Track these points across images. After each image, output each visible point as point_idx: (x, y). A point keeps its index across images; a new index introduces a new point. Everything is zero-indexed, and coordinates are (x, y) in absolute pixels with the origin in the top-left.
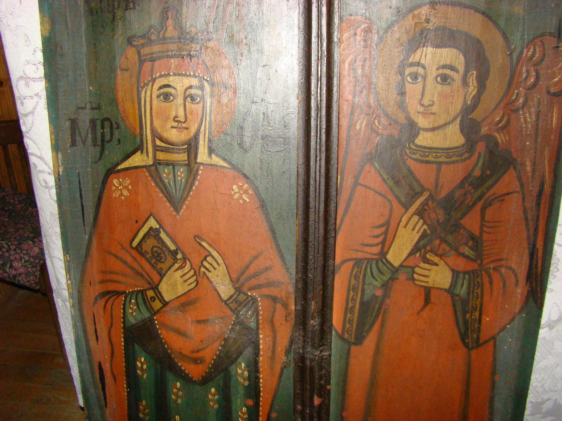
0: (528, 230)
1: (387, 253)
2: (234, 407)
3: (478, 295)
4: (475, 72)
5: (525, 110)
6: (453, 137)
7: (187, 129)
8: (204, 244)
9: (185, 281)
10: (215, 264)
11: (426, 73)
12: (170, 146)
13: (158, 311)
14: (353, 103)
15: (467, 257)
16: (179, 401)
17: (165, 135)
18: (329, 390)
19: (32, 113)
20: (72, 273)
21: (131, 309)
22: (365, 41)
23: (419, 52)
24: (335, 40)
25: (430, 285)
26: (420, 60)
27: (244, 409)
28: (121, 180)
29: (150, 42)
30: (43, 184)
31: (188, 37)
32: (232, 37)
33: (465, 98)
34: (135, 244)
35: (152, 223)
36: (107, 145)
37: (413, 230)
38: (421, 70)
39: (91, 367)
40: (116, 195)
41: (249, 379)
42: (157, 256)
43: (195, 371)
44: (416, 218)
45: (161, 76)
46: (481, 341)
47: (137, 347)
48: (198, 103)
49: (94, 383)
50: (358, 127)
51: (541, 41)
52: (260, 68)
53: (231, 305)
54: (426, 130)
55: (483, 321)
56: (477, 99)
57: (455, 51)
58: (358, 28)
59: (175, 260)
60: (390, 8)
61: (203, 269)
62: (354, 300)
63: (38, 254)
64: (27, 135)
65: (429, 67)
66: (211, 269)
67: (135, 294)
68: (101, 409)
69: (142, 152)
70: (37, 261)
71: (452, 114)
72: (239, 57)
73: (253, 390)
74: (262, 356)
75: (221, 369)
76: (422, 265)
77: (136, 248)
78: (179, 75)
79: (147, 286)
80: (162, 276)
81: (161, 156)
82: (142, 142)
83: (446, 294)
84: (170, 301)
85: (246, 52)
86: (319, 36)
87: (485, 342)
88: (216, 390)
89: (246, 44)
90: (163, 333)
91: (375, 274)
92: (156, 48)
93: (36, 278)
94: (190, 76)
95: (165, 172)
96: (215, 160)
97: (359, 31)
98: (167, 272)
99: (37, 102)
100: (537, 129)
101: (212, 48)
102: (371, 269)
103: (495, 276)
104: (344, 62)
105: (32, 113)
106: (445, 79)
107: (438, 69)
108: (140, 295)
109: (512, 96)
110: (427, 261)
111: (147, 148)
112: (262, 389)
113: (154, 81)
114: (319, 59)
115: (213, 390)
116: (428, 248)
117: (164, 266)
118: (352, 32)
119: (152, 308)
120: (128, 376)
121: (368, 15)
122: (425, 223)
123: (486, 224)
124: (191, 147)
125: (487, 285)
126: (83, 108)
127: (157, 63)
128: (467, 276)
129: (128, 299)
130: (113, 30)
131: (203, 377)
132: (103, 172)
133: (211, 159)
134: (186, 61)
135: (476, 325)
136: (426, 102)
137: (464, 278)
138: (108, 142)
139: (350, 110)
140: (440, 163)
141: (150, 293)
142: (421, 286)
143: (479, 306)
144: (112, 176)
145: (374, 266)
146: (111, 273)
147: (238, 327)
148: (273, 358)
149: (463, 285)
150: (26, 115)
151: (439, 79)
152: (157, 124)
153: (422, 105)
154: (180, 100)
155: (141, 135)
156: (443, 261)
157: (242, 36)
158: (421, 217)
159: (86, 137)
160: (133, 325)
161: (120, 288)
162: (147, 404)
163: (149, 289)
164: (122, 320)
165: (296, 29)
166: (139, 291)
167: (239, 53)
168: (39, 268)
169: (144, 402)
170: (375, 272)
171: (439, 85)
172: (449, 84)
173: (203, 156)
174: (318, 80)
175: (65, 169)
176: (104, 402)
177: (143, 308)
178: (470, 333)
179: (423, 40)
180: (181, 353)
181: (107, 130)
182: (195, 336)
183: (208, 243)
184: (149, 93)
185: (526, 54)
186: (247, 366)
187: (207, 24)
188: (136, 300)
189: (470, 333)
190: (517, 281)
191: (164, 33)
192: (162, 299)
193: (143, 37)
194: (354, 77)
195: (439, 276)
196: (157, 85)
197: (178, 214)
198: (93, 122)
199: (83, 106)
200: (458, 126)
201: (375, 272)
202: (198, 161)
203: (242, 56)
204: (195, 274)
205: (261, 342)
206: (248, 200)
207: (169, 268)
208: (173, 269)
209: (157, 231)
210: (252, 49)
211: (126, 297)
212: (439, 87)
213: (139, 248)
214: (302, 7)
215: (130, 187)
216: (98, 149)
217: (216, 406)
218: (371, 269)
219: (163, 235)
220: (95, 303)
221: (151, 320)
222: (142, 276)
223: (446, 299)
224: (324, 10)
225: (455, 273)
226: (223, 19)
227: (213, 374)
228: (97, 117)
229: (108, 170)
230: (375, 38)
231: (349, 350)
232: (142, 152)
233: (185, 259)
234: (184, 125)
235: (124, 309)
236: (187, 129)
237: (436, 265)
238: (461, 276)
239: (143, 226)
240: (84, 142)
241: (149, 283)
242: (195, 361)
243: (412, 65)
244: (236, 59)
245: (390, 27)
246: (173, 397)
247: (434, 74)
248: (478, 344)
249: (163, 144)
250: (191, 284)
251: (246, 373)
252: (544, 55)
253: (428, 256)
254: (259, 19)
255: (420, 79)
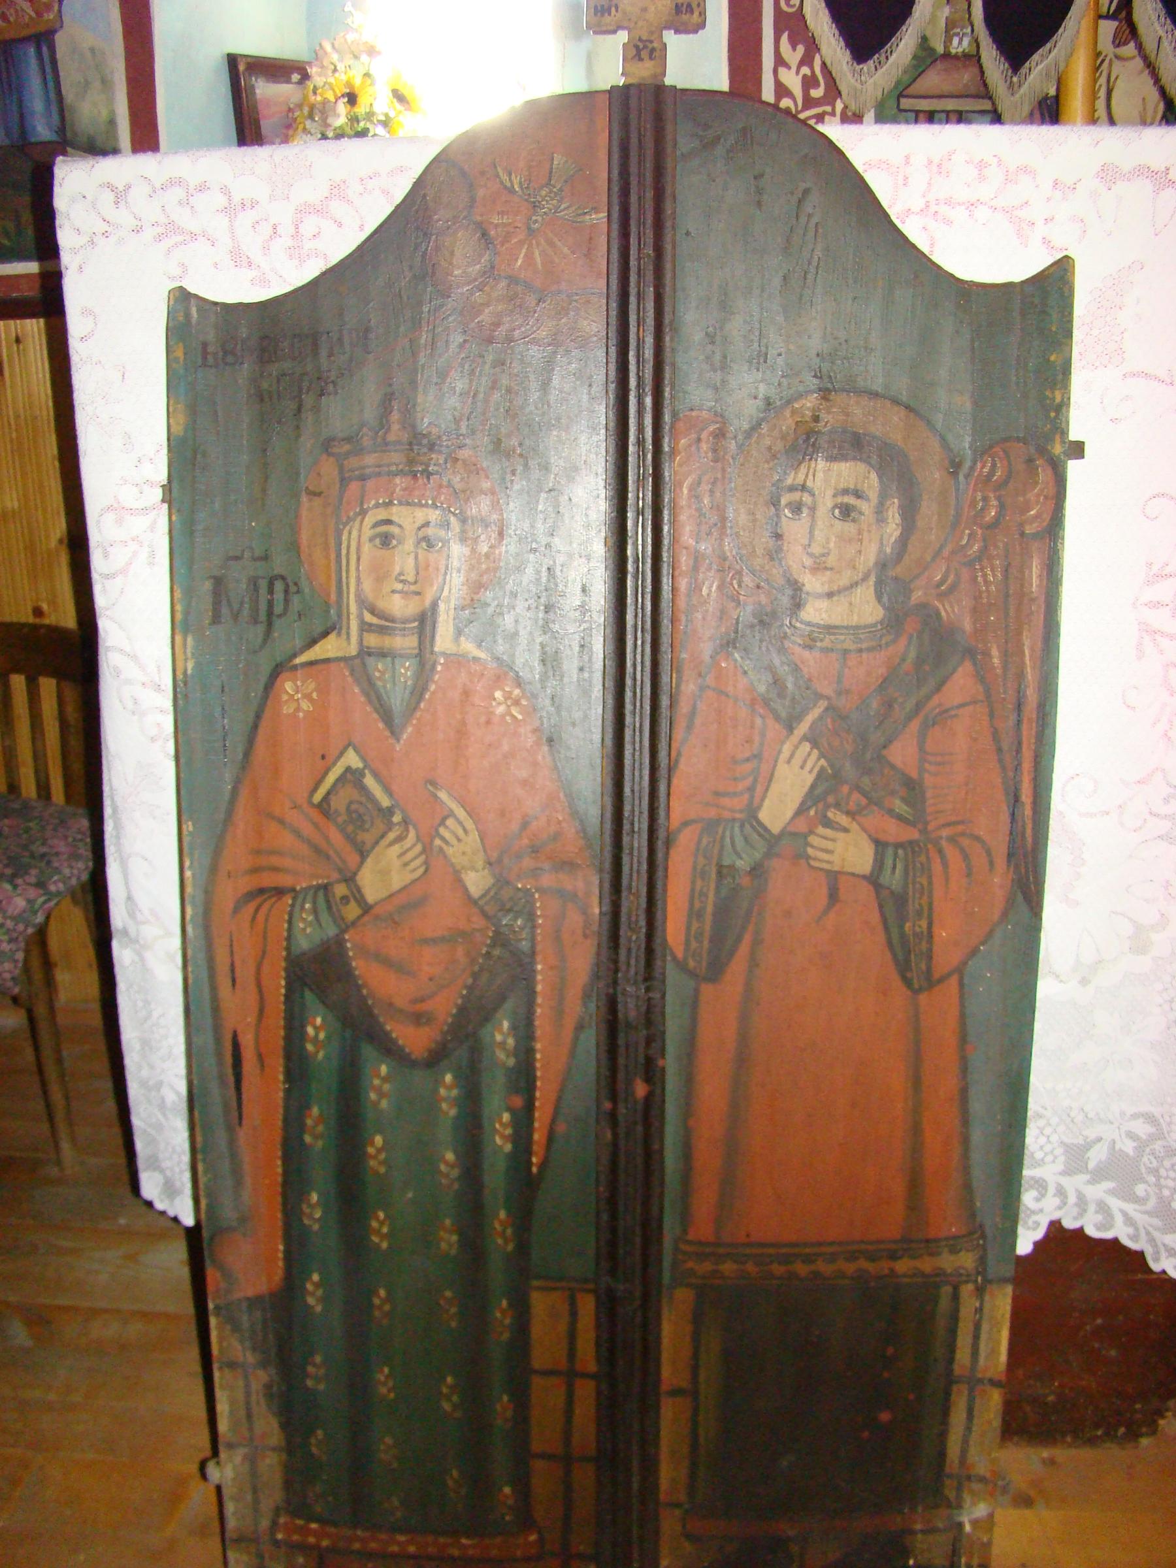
0: (1004, 768)
1: (759, 807)
2: (486, 1112)
3: (923, 888)
4: (896, 500)
5: (985, 562)
6: (866, 608)
7: (418, 593)
8: (443, 795)
9: (406, 864)
10: (460, 832)
11: (814, 502)
12: (385, 624)
13: (354, 923)
14: (697, 551)
15: (900, 818)
16: (384, 1104)
17: (381, 604)
18: (663, 1069)
19: (124, 571)
20: (196, 856)
21: (304, 920)
22: (715, 451)
23: (803, 469)
24: (666, 449)
25: (836, 869)
26: (805, 481)
27: (506, 1117)
28: (299, 683)
29: (359, 451)
30: (130, 705)
31: (425, 442)
32: (498, 443)
33: (882, 543)
34: (318, 797)
35: (352, 759)
36: (278, 623)
37: (802, 767)
38: (807, 498)
39: (218, 1039)
40: (287, 709)
41: (516, 1052)
42: (357, 821)
43: (414, 1039)
44: (806, 746)
45: (377, 506)
46: (936, 976)
47: (309, 996)
48: (438, 551)
49: (221, 1077)
50: (705, 591)
51: (1004, 451)
52: (543, 495)
53: (487, 908)
54: (819, 596)
55: (936, 939)
56: (903, 542)
57: (861, 467)
58: (703, 430)
59: (390, 826)
60: (755, 398)
61: (438, 842)
62: (703, 894)
63: (24, 911)
64: (107, 613)
65: (820, 494)
66: (454, 841)
67: (312, 892)
68: (230, 1129)
69: (339, 634)
70: (21, 927)
71: (862, 568)
72: (509, 477)
73: (524, 1077)
74: (540, 1005)
75: (461, 1040)
76: (821, 830)
77: (319, 806)
78: (408, 504)
79: (335, 876)
80: (363, 855)
81: (372, 640)
82: (339, 616)
83: (865, 883)
84: (376, 904)
85: (520, 468)
86: (640, 442)
87: (941, 980)
88: (455, 1077)
89: (521, 455)
90: (359, 966)
91: (739, 848)
92: (369, 460)
93: (16, 967)
94: (426, 505)
95: (378, 667)
96: (468, 646)
97: (704, 435)
98: (373, 848)
99: (135, 554)
100: (1007, 596)
101: (464, 461)
102: (732, 838)
103: (951, 852)
104: (681, 485)
105: (124, 571)
106: (846, 512)
107: (834, 496)
108: (321, 894)
109: (962, 538)
110: (828, 823)
111: (348, 628)
112: (539, 1074)
113: (363, 513)
114: (639, 481)
115: (448, 1078)
116: (831, 799)
117: (367, 837)
118: (694, 436)
119: (343, 919)
120: (288, 1057)
121: (719, 410)
122: (822, 755)
123: (931, 758)
124: (425, 622)
125: (937, 867)
126: (236, 558)
127: (370, 484)
128: (900, 852)
129: (299, 900)
130: (298, 427)
131: (430, 1051)
132: (266, 669)
133: (459, 645)
134: (420, 481)
135: (924, 946)
136: (816, 549)
137: (896, 855)
138: (280, 616)
139: (691, 562)
140: (846, 652)
141: (340, 890)
142: (821, 869)
143: (926, 908)
144: (284, 675)
145: (737, 830)
146: (272, 852)
147: (497, 952)
148: (559, 1012)
149: (894, 868)
150: (107, 577)
151: (837, 511)
152: (367, 586)
153: (811, 555)
154: (409, 545)
155: (339, 603)
156: (859, 824)
157: (514, 442)
158: (815, 744)
159: (239, 611)
160: (304, 954)
161: (285, 880)
162: (321, 1115)
163: (338, 881)
164: (285, 944)
165: (603, 431)
166: (318, 888)
167: (509, 470)
168: (22, 945)
169: (315, 1111)
170: (739, 840)
171: (837, 521)
172: (854, 521)
173: (443, 640)
174: (638, 515)
175: (198, 665)
176: (236, 1114)
177: (325, 917)
178: (912, 963)
179: (811, 449)
180: (391, 1004)
181: (279, 596)
182: (413, 983)
183: (450, 795)
184: (355, 534)
185: (981, 471)
186: (514, 1028)
187: (457, 421)
188: (314, 902)
189: (912, 963)
190: (991, 863)
191: (386, 433)
192: (361, 900)
193: (348, 440)
194: (697, 510)
195: (849, 850)
196: (369, 520)
197: (398, 740)
198: (254, 582)
199: (238, 554)
200: (872, 589)
201: (739, 840)
202: (436, 649)
203: (514, 474)
204: (424, 851)
205: (539, 977)
206: (520, 717)
207: (377, 843)
208: (384, 843)
209: (360, 774)
210: (530, 463)
211: (294, 899)
212: (838, 525)
213: (325, 806)
214: (612, 396)
215: (315, 695)
216: (261, 629)
217: (453, 1112)
218: (732, 838)
219: (369, 781)
220: (236, 911)
221: (340, 942)
222: (328, 858)
223: (865, 892)
224: (648, 401)
225: (880, 845)
226: (484, 414)
227: (450, 1046)
228: (260, 573)
229: (277, 666)
230: (733, 446)
231: (697, 991)
232: (339, 634)
233: (405, 822)
234: (413, 588)
235: (290, 922)
236: (418, 593)
237: (846, 830)
238: (890, 851)
239: (335, 763)
240: (236, 617)
241: (340, 871)
242: (419, 1019)
243: (792, 489)
244: (504, 479)
245: (755, 427)
246: (373, 1096)
247: (830, 504)
248: (931, 982)
249: (375, 620)
250: (415, 870)
251: (511, 1042)
252: (1010, 472)
253: (830, 814)
254: (543, 414)
255: (805, 512)
